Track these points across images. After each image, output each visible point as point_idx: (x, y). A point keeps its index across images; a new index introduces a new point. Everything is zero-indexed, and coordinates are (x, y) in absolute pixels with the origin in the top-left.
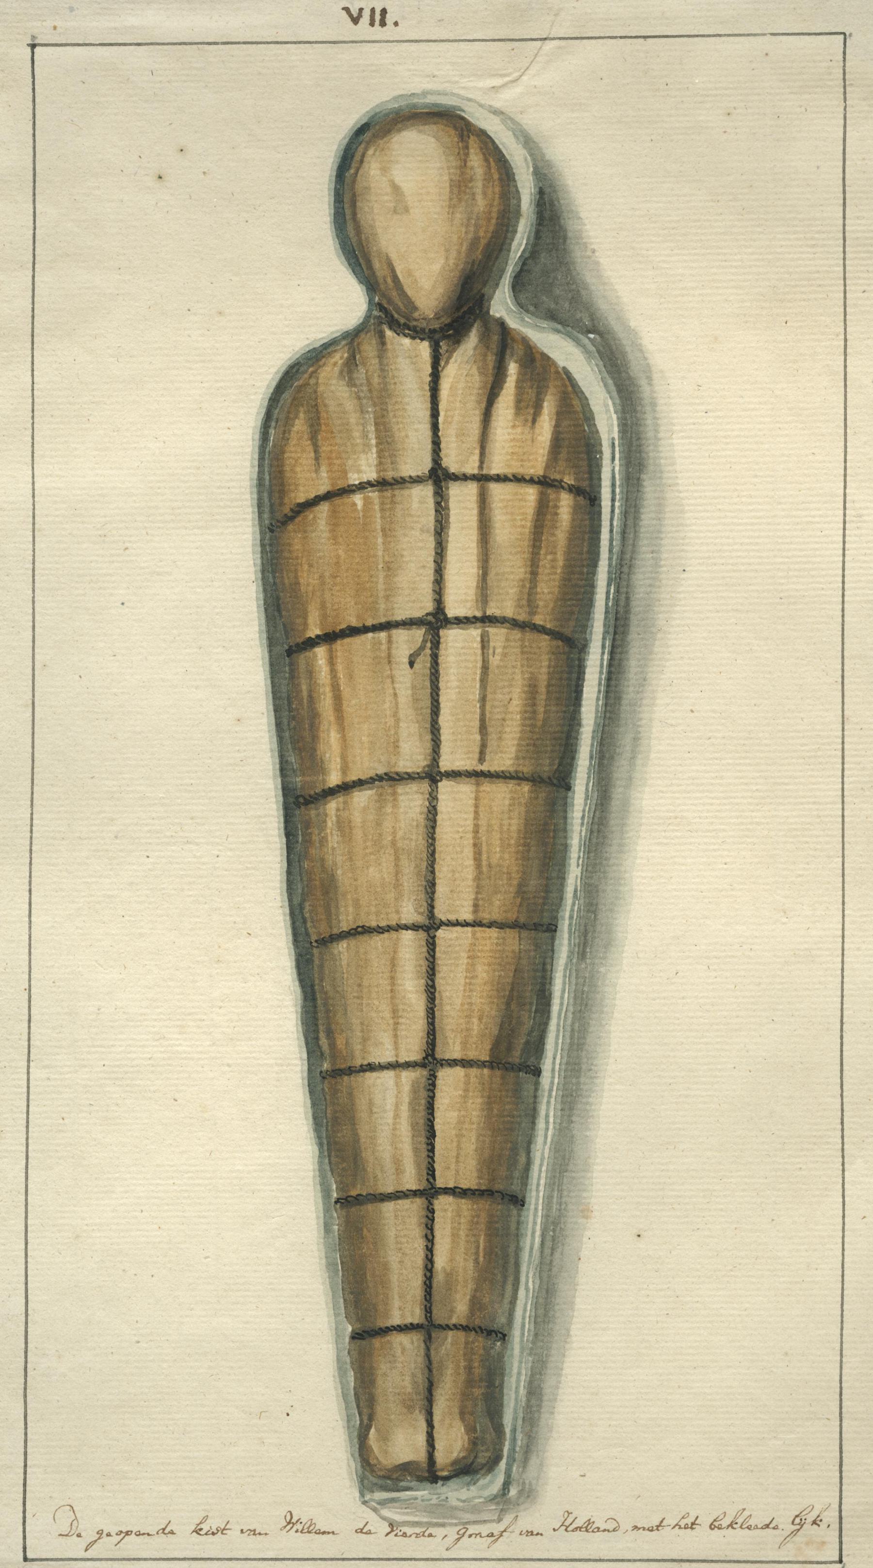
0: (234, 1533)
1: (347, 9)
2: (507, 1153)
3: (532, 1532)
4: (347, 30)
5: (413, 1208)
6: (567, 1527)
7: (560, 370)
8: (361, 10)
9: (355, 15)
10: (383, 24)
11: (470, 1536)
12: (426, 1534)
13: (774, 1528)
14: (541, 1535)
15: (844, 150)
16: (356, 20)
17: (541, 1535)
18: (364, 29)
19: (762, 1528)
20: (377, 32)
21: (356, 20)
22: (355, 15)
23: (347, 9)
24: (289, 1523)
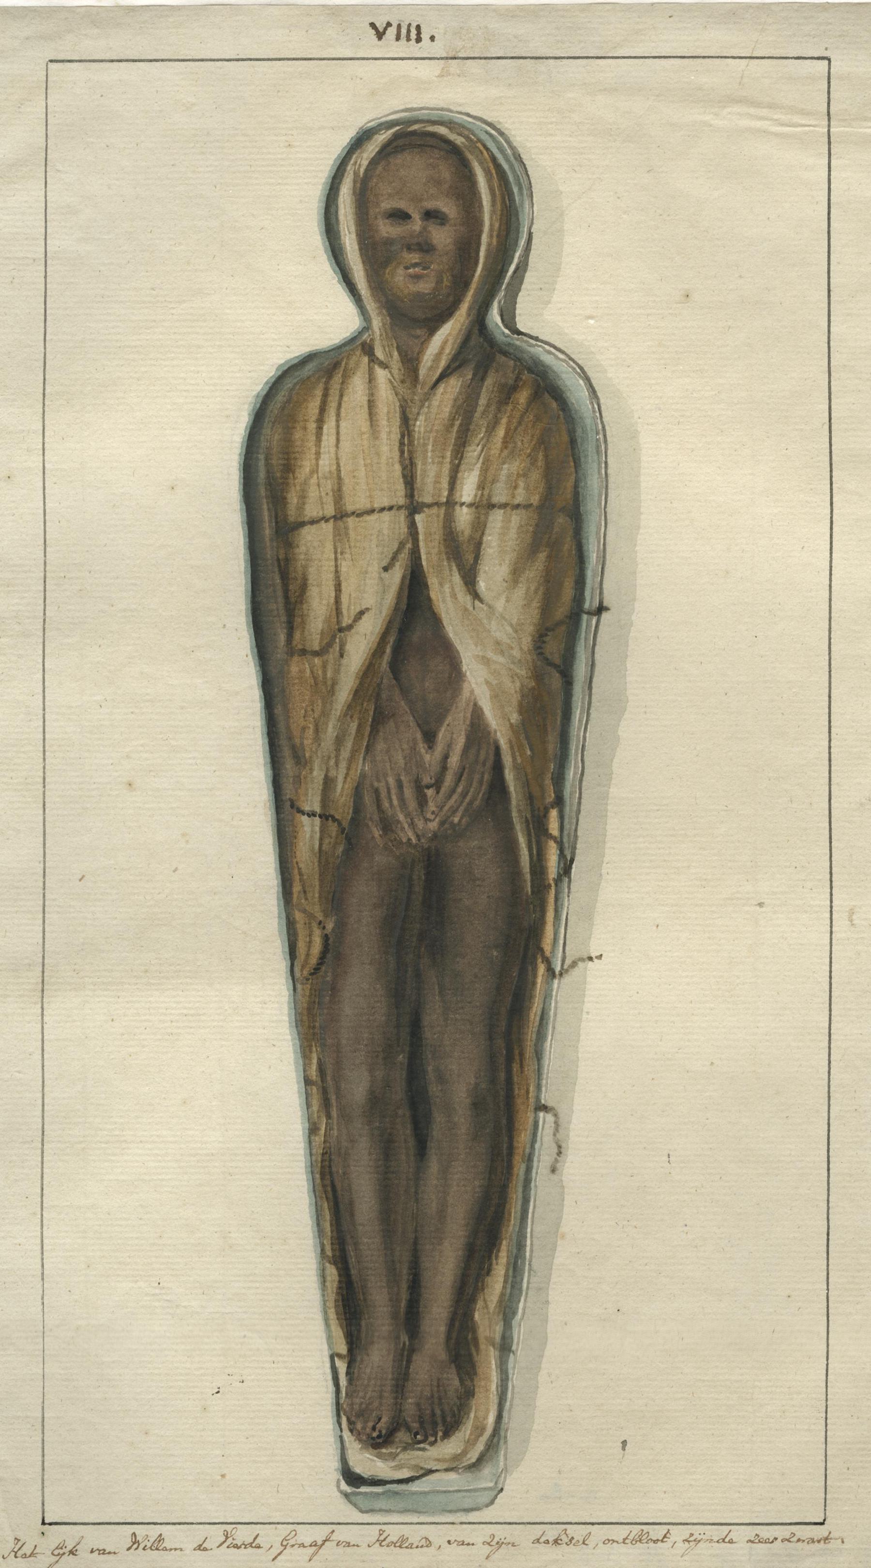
0: (189, 1546)
1: (373, 25)
2: (456, 1054)
3: (463, 1542)
4: (370, 45)
5: (356, 500)
6: (16, 1553)
7: (491, 741)
8: (389, 24)
9: (381, 30)
10: (419, 40)
11: (293, 1546)
12: (727, 1540)
13: (729, 1542)
14: (358, 1546)
15: (831, 553)
16: (380, 35)
17: (358, 1546)
18: (390, 46)
19: (718, 1542)
20: (413, 49)
21: (380, 35)
22: (381, 30)
23: (373, 25)
24: (134, 1543)
